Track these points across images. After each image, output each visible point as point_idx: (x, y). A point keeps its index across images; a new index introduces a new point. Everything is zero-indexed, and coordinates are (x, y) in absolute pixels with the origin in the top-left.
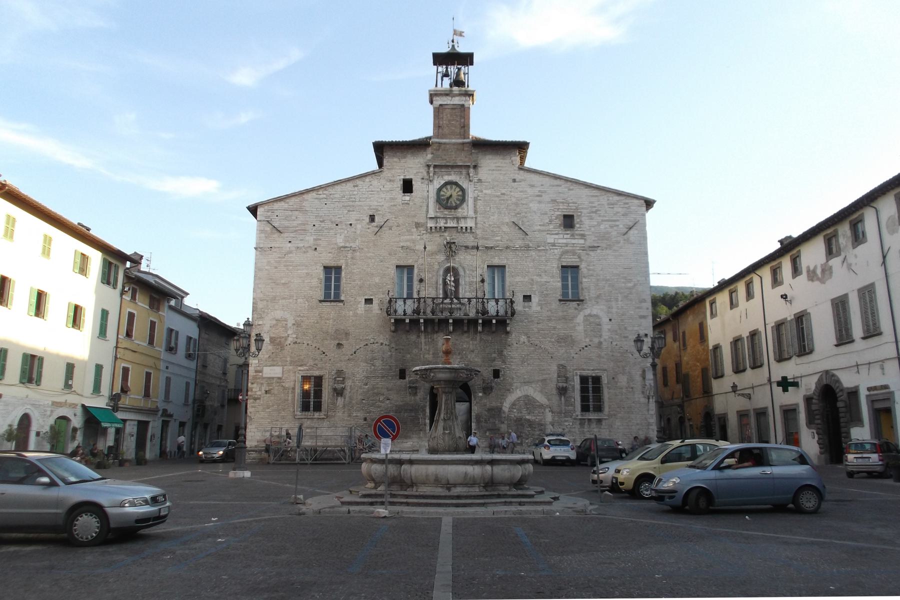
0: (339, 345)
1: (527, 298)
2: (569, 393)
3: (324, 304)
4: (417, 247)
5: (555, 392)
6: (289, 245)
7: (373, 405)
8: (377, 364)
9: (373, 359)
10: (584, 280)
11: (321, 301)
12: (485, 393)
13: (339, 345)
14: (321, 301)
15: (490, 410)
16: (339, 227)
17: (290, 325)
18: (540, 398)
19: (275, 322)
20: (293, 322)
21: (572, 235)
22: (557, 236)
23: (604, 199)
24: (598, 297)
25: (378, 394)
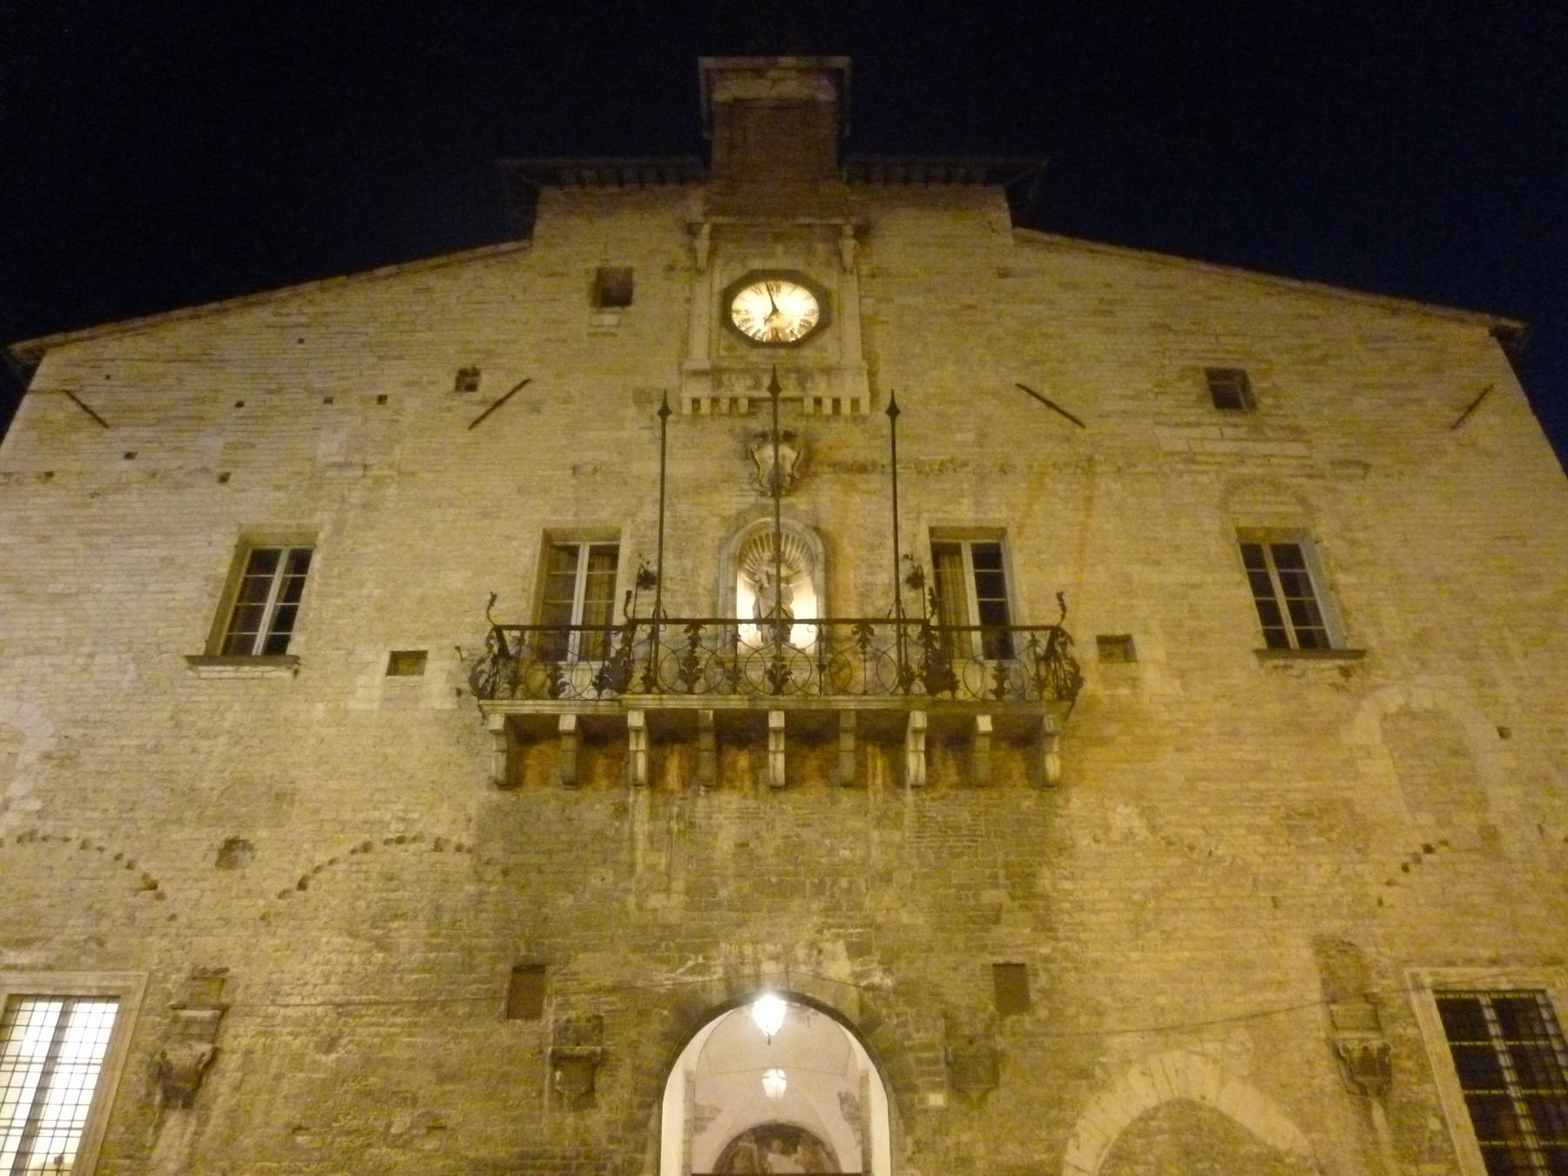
0: (231, 852)
1: (1117, 647)
2: (1405, 1085)
4: (636, 467)
5: (1327, 1077)
6: (126, 464)
8: (404, 942)
11: (194, 661)
13: (382, 399)
14: (194, 661)
20: (49, 744)
22: (1196, 433)
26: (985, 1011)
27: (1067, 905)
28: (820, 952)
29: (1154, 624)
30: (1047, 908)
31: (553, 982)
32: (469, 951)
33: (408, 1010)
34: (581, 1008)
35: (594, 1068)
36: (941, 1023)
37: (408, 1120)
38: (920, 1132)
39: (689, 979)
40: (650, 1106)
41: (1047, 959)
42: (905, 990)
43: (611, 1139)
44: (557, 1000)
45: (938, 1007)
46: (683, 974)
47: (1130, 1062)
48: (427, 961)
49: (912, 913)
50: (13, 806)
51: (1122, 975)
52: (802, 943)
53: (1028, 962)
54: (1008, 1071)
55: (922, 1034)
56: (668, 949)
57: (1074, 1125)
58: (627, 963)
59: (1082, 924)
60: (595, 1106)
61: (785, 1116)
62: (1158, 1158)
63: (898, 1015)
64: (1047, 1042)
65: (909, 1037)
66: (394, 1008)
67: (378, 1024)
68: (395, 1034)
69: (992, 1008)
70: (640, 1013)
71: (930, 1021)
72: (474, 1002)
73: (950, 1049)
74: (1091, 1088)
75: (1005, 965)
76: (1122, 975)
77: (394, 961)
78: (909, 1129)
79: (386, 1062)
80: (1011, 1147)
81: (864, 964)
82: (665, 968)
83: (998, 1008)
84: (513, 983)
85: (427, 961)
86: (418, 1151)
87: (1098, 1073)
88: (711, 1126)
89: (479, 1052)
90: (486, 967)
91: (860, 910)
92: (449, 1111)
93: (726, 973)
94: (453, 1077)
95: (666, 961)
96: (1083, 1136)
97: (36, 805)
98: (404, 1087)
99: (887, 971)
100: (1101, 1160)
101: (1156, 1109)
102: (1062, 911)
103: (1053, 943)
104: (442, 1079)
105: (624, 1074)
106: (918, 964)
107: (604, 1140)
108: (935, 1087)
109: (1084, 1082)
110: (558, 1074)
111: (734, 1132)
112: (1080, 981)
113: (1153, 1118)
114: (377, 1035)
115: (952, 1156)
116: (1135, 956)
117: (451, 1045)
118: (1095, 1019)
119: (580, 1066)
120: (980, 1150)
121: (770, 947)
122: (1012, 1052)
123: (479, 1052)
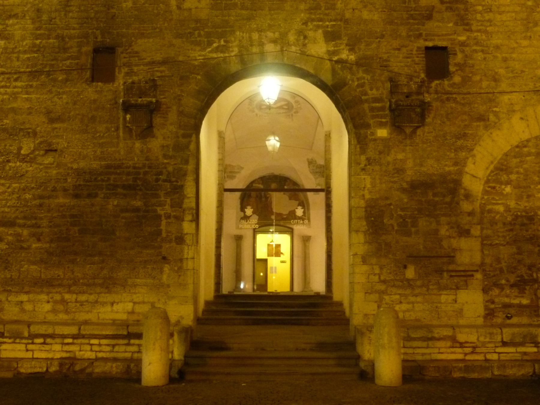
8: (18, 34)
12: (397, 126)
15: (417, 187)
26: (418, 77)
27: (480, 8)
28: (305, 37)
30: (466, 10)
31: (122, 58)
32: (61, 38)
33: (24, 77)
34: (141, 74)
35: (152, 112)
36: (388, 85)
37: (32, 146)
38: (371, 153)
39: (215, 55)
40: (190, 136)
41: (463, 44)
42: (363, 63)
43: (165, 156)
44: (125, 70)
45: (386, 74)
46: (210, 52)
47: (514, 111)
48: (34, 45)
49: (371, 11)
51: (514, 56)
52: (292, 32)
53: (449, 46)
54: (432, 115)
55: (374, 91)
56: (200, 35)
57: (472, 150)
58: (172, 45)
59: (489, 21)
60: (154, 136)
61: (280, 168)
62: (526, 170)
63: (358, 79)
64: (459, 98)
65: (366, 94)
66: (15, 76)
67: (6, 87)
68: (18, 93)
69: (423, 75)
70: (182, 78)
71: (380, 84)
72: (68, 71)
73: (393, 101)
74: (486, 128)
75: (435, 48)
76: (514, 56)
77: (12, 46)
78: (363, 151)
79: (14, 110)
80: (431, 162)
81: (336, 46)
82: (198, 48)
83: (427, 76)
84: (94, 59)
85: (34, 45)
86: (41, 164)
87: (492, 117)
88: (237, 176)
89: (75, 103)
90: (75, 49)
91: (334, 9)
92: (58, 140)
93: (240, 51)
94: (59, 119)
95: (198, 44)
96: (479, 157)
98: (27, 126)
99: (352, 50)
100: (489, 172)
101: (528, 141)
102: (476, 12)
103: (468, 34)
104: (52, 121)
105: (173, 116)
106: (374, 46)
107: (160, 157)
108: (382, 125)
109: (482, 123)
110: (128, 117)
111: (252, 179)
112: (485, 59)
113: (525, 147)
114: (6, 93)
115: (391, 167)
116: (525, 43)
117: (56, 99)
118: (493, 84)
119: (141, 112)
120: (410, 164)
121: (270, 34)
122: (435, 104)
123: (75, 103)
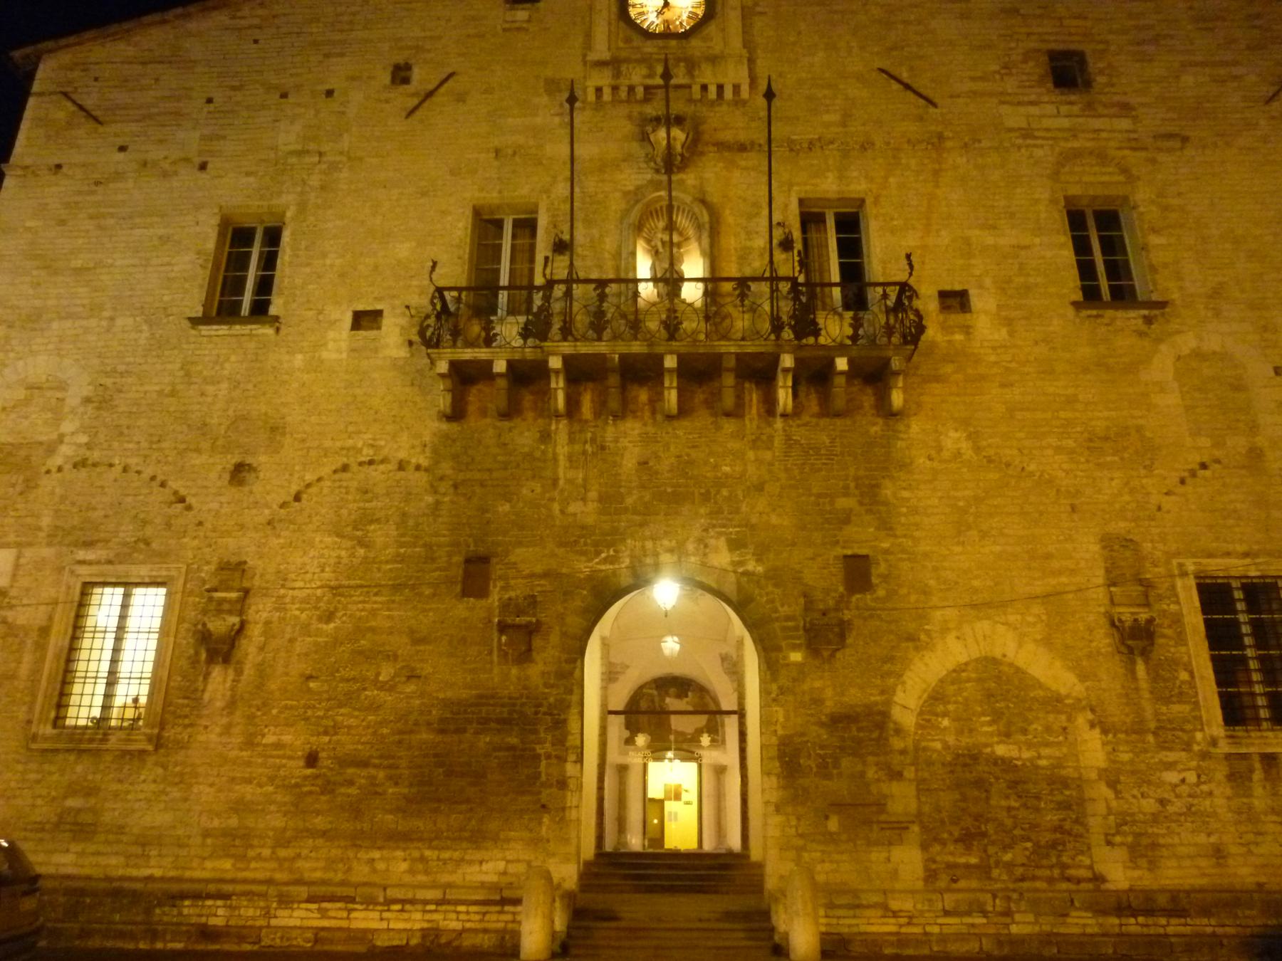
0: (240, 473)
1: (955, 300)
2: (1165, 647)
3: (205, 330)
4: (549, 149)
5: (1103, 640)
7: (348, 699)
9: (365, 519)
10: (1154, 240)
11: (195, 322)
14: (195, 322)
15: (840, 720)
16: (291, 99)
17: (73, 399)
18: (1048, 671)
19: (21, 394)
20: (87, 391)
21: (1089, 106)
22: (1033, 110)
23: (578, 736)
24: (1216, 293)
25: (368, 656)
29: (988, 282)
50: (66, 439)
97: (83, 439)
